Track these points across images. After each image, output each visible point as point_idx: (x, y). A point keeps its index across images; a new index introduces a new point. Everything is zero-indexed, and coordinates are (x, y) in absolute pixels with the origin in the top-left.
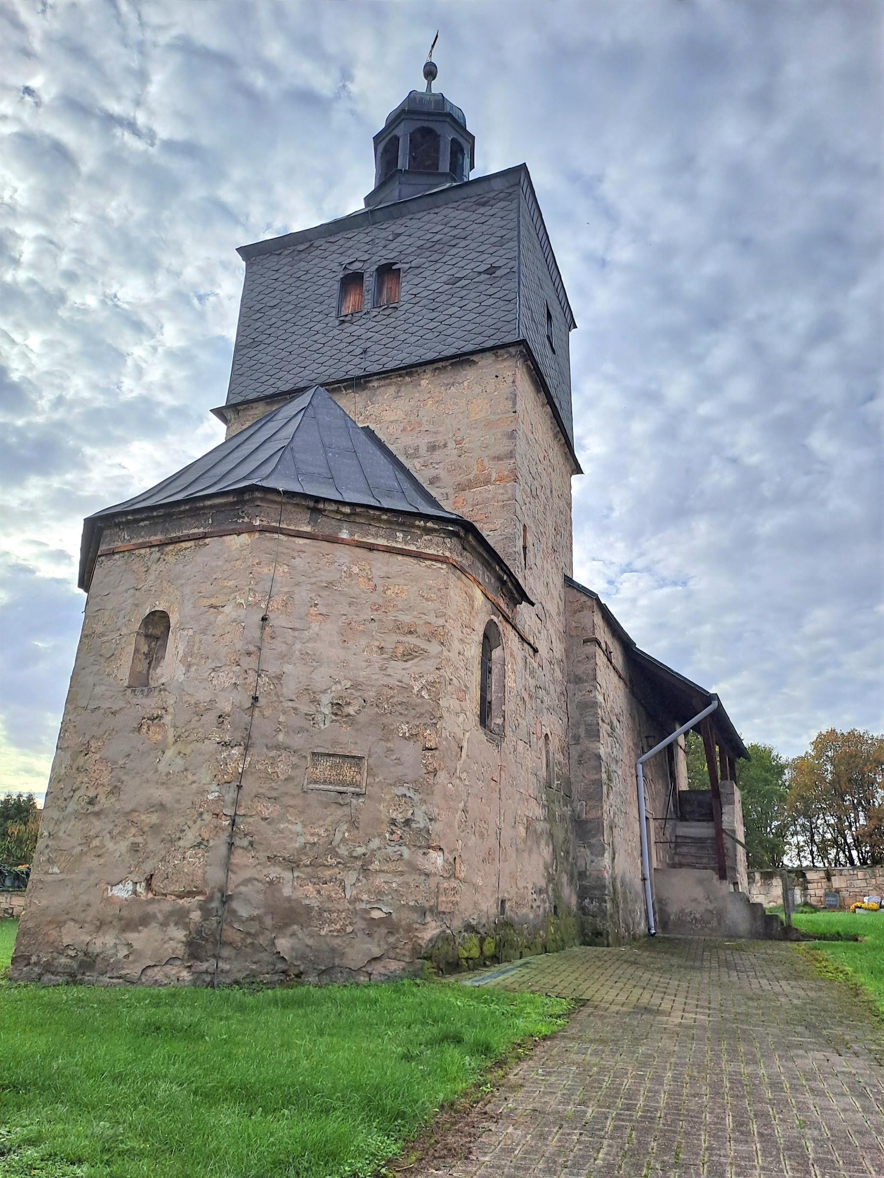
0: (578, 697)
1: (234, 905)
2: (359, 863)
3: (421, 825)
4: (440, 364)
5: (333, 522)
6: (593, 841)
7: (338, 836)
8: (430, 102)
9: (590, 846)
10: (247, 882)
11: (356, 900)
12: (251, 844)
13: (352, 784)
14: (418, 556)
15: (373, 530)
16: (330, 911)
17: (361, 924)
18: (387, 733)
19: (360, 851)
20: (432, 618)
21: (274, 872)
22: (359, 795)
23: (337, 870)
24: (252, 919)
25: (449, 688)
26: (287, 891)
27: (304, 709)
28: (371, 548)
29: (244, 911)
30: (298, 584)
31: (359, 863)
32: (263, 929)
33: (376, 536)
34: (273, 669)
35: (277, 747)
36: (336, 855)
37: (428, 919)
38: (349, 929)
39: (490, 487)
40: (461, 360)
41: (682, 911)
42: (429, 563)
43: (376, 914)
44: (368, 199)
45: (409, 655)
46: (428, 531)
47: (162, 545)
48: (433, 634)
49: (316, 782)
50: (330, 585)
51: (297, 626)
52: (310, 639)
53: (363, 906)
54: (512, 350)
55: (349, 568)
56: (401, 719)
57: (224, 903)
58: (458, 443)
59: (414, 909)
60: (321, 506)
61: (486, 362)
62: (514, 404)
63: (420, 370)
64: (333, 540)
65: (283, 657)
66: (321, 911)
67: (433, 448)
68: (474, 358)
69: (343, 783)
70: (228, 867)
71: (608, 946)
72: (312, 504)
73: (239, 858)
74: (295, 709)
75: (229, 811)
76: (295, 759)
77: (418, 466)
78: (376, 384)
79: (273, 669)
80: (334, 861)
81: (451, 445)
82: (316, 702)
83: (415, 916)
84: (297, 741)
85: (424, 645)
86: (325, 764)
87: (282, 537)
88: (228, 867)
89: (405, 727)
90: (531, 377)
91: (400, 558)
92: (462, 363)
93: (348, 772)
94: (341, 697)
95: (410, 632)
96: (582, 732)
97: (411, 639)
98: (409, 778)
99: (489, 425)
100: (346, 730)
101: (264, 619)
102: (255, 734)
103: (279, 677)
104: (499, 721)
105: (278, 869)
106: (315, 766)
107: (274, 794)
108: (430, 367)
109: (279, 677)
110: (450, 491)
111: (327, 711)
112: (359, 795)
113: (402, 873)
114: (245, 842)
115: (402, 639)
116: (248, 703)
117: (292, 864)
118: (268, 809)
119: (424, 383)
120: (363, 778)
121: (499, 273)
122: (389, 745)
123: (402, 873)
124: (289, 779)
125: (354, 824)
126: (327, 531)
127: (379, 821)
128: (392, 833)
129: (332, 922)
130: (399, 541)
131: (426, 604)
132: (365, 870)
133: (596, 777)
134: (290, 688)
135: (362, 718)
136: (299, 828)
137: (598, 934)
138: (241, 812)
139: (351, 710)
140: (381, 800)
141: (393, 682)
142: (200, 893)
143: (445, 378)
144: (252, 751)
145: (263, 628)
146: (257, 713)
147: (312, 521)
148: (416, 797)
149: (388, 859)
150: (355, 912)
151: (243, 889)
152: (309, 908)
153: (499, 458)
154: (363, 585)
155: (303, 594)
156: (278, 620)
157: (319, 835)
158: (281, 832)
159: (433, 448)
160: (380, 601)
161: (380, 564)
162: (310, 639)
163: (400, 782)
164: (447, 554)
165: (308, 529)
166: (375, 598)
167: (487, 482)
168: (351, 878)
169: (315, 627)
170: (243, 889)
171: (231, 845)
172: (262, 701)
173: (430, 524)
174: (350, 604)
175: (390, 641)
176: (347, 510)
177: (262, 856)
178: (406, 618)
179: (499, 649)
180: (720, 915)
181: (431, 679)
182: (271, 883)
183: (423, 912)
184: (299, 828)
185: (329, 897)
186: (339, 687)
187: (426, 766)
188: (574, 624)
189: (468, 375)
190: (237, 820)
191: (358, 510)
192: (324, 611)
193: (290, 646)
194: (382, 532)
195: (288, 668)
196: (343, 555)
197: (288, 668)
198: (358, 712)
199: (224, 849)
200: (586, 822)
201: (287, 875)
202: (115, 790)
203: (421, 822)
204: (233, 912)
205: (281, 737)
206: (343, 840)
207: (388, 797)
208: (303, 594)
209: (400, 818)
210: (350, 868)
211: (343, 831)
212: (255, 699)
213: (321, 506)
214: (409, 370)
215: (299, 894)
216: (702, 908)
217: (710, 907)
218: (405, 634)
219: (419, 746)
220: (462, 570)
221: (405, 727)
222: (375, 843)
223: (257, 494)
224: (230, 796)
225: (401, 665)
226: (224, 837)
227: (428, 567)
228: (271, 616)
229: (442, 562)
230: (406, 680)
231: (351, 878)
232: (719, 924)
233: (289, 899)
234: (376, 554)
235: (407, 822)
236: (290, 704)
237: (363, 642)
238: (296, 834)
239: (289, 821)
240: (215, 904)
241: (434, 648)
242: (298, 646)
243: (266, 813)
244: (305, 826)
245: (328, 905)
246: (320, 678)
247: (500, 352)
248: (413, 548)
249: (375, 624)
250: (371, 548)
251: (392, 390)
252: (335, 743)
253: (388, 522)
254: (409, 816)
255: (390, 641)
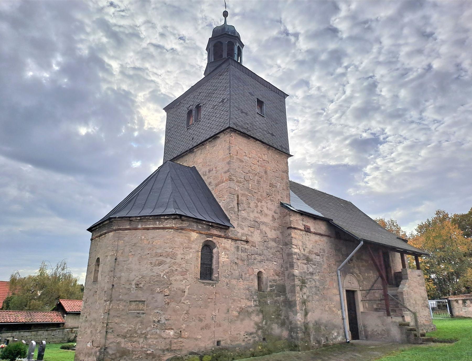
0: (287, 252)
1: (108, 350)
2: (144, 335)
3: (163, 322)
4: (210, 140)
5: (136, 223)
6: (293, 309)
7: (137, 327)
8: (220, 30)
9: (293, 311)
10: (111, 343)
11: (142, 348)
12: (113, 331)
13: (141, 310)
14: (164, 228)
15: (149, 223)
16: (135, 351)
17: (144, 355)
18: (152, 291)
19: (144, 332)
20: (168, 250)
21: (119, 340)
22: (143, 313)
23: (137, 338)
24: (113, 354)
25: (176, 273)
26: (123, 345)
27: (127, 287)
28: (148, 229)
29: (111, 352)
30: (126, 246)
31: (144, 335)
32: (116, 358)
33: (150, 224)
34: (118, 275)
35: (120, 300)
36: (137, 334)
37: (166, 353)
38: (141, 357)
39: (224, 184)
40: (215, 137)
41: (373, 330)
42: (167, 230)
43: (149, 352)
44: (204, 74)
45: (160, 264)
46: (166, 219)
47: (100, 236)
48: (168, 255)
49: (131, 310)
50: (135, 245)
51: (125, 260)
52: (129, 264)
53: (145, 349)
54: (228, 130)
55: (141, 237)
56: (157, 286)
57: (105, 349)
58: (216, 168)
59: (160, 350)
60: (131, 219)
61: (222, 136)
62: (230, 150)
63: (205, 143)
64: (136, 229)
65: (121, 271)
66: (133, 351)
67: (210, 171)
68: (218, 136)
69: (139, 310)
70: (106, 338)
71: (299, 351)
72: (128, 219)
73: (109, 336)
74: (125, 287)
75: (106, 322)
76: (124, 304)
77: (206, 178)
78: (195, 150)
79: (118, 275)
80: (136, 335)
81: (214, 169)
82: (131, 284)
83: (161, 352)
84: (125, 297)
85: (164, 259)
86: (134, 304)
87: (120, 231)
88: (106, 338)
89: (158, 289)
90: (242, 135)
91: (158, 230)
92: (215, 138)
93: (141, 306)
94: (138, 282)
95: (161, 256)
96: (288, 266)
97: (161, 258)
98: (160, 306)
99: (223, 159)
100: (140, 292)
101: (116, 259)
102: (113, 296)
103: (120, 278)
104: (216, 275)
105: (120, 339)
106: (131, 305)
107: (119, 315)
108: (207, 142)
109: (120, 278)
110: (214, 187)
111: (134, 286)
112: (143, 313)
113: (157, 338)
114: (111, 331)
115: (159, 258)
116: (111, 287)
117: (124, 337)
118: (117, 320)
119: (207, 147)
120: (145, 308)
121: (225, 101)
122: (153, 296)
123: (157, 338)
124: (123, 310)
125: (142, 323)
126: (134, 226)
127: (150, 322)
128: (154, 325)
129: (136, 355)
130: (158, 224)
131: (166, 245)
132: (146, 338)
133: (293, 283)
134: (123, 281)
135: (145, 288)
136: (126, 325)
137: (296, 346)
138: (110, 321)
139: (141, 286)
140: (150, 315)
141: (155, 274)
142: (99, 347)
143: (212, 144)
144: (113, 302)
145: (116, 262)
146: (114, 290)
147: (130, 224)
148: (162, 313)
149: (152, 334)
150: (142, 352)
151: (110, 345)
152: (129, 351)
153: (225, 172)
154: (145, 242)
155: (127, 249)
156: (120, 259)
157: (132, 327)
158: (121, 327)
159: (210, 171)
160: (151, 247)
161: (151, 233)
162: (129, 264)
163: (157, 308)
164: (174, 226)
165: (128, 227)
166: (150, 246)
167: (223, 182)
168: (141, 340)
169: (131, 259)
170: (110, 345)
171: (107, 332)
172: (115, 286)
173: (166, 217)
174: (142, 249)
175: (154, 260)
176: (139, 218)
177: (116, 335)
178: (159, 251)
179: (216, 249)
180: (388, 332)
181: (167, 271)
182: (118, 343)
183: (164, 351)
184: (126, 325)
185: (135, 347)
186: (138, 278)
187: (165, 301)
188: (284, 222)
189: (218, 141)
190: (109, 324)
191: (142, 218)
192: (133, 254)
193: (123, 267)
194: (152, 223)
195: (123, 274)
196: (139, 233)
197: (123, 274)
198: (144, 286)
199: (105, 333)
200: (292, 302)
201: (123, 340)
202: (90, 314)
203: (163, 321)
204: (107, 352)
205: (121, 297)
206: (139, 328)
207: (153, 313)
208: (127, 249)
209: (156, 320)
210: (141, 337)
211: (139, 326)
212: (113, 285)
213: (131, 219)
214: (202, 143)
215: (126, 346)
216: (380, 329)
217: (384, 328)
218: (159, 257)
219: (163, 295)
220: (182, 229)
221: (158, 289)
222: (149, 329)
223: (113, 219)
224: (106, 317)
225: (158, 267)
226: (105, 329)
227: (167, 232)
228: (118, 258)
229: (172, 229)
230: (159, 273)
231: (141, 340)
232: (388, 336)
233: (123, 348)
234: (150, 231)
235: (159, 321)
236: (123, 286)
237: (145, 262)
238: (125, 327)
239: (123, 324)
240: (103, 350)
241: (168, 260)
242: (125, 266)
243: (116, 321)
244: (127, 325)
245: (134, 349)
246: (132, 276)
247: (225, 132)
248: (162, 226)
249: (149, 255)
250: (148, 229)
251: (200, 151)
252: (137, 297)
253: (152, 219)
254: (159, 319)
255: (154, 260)
